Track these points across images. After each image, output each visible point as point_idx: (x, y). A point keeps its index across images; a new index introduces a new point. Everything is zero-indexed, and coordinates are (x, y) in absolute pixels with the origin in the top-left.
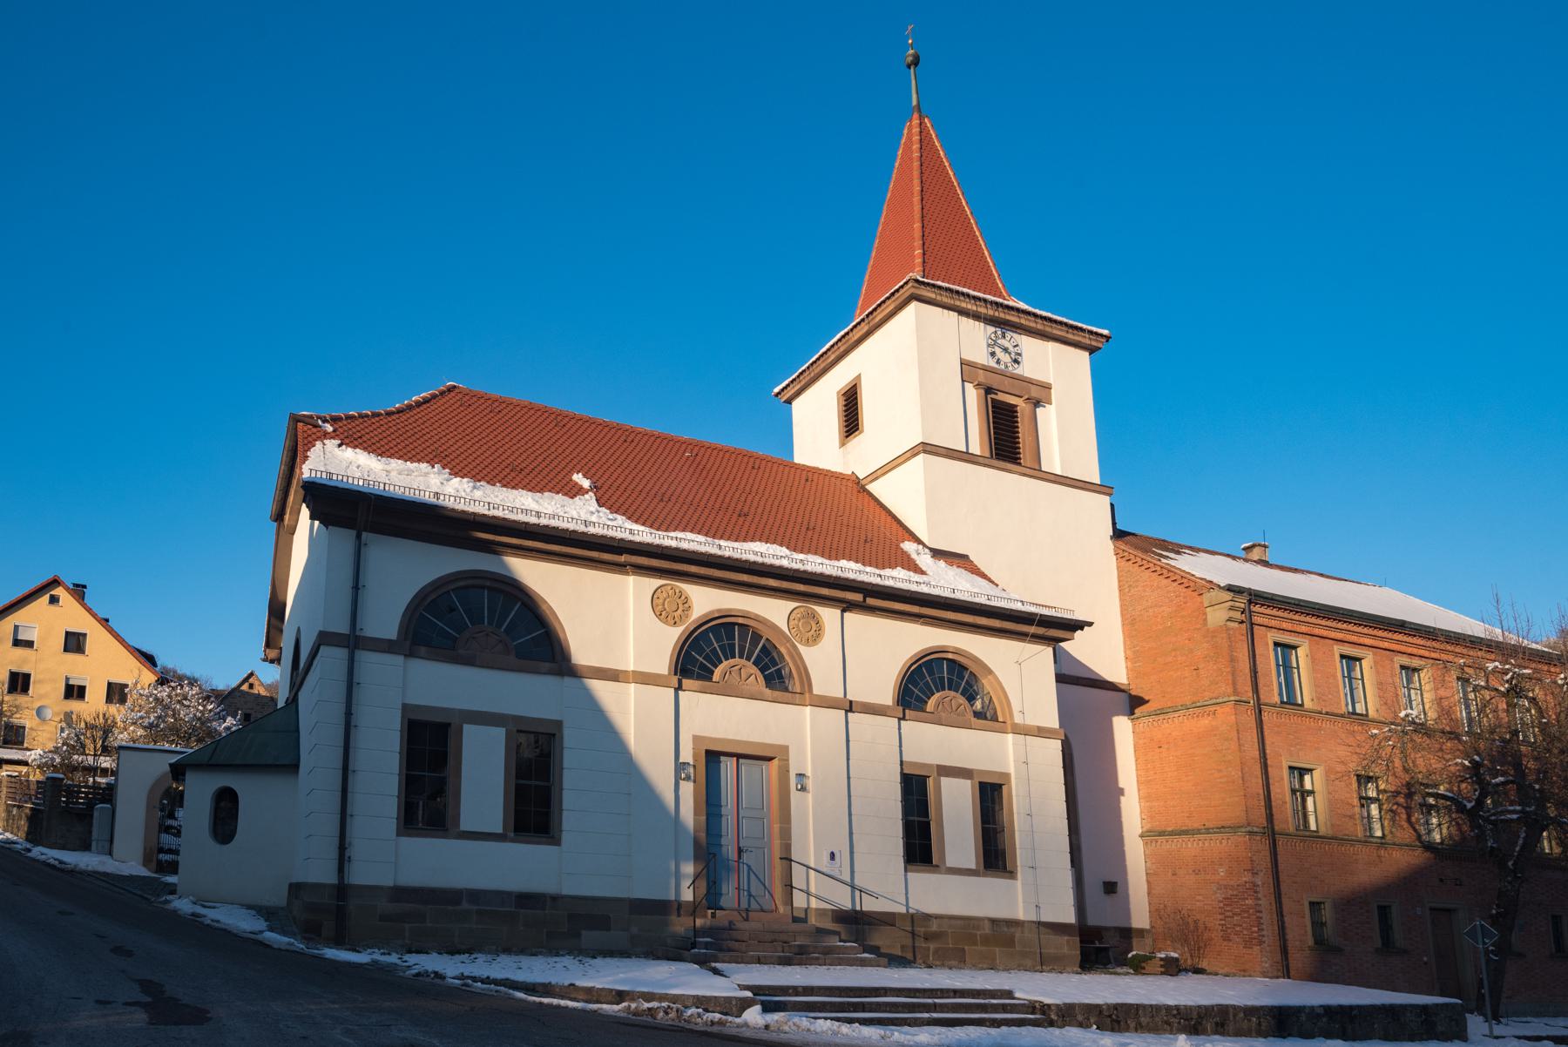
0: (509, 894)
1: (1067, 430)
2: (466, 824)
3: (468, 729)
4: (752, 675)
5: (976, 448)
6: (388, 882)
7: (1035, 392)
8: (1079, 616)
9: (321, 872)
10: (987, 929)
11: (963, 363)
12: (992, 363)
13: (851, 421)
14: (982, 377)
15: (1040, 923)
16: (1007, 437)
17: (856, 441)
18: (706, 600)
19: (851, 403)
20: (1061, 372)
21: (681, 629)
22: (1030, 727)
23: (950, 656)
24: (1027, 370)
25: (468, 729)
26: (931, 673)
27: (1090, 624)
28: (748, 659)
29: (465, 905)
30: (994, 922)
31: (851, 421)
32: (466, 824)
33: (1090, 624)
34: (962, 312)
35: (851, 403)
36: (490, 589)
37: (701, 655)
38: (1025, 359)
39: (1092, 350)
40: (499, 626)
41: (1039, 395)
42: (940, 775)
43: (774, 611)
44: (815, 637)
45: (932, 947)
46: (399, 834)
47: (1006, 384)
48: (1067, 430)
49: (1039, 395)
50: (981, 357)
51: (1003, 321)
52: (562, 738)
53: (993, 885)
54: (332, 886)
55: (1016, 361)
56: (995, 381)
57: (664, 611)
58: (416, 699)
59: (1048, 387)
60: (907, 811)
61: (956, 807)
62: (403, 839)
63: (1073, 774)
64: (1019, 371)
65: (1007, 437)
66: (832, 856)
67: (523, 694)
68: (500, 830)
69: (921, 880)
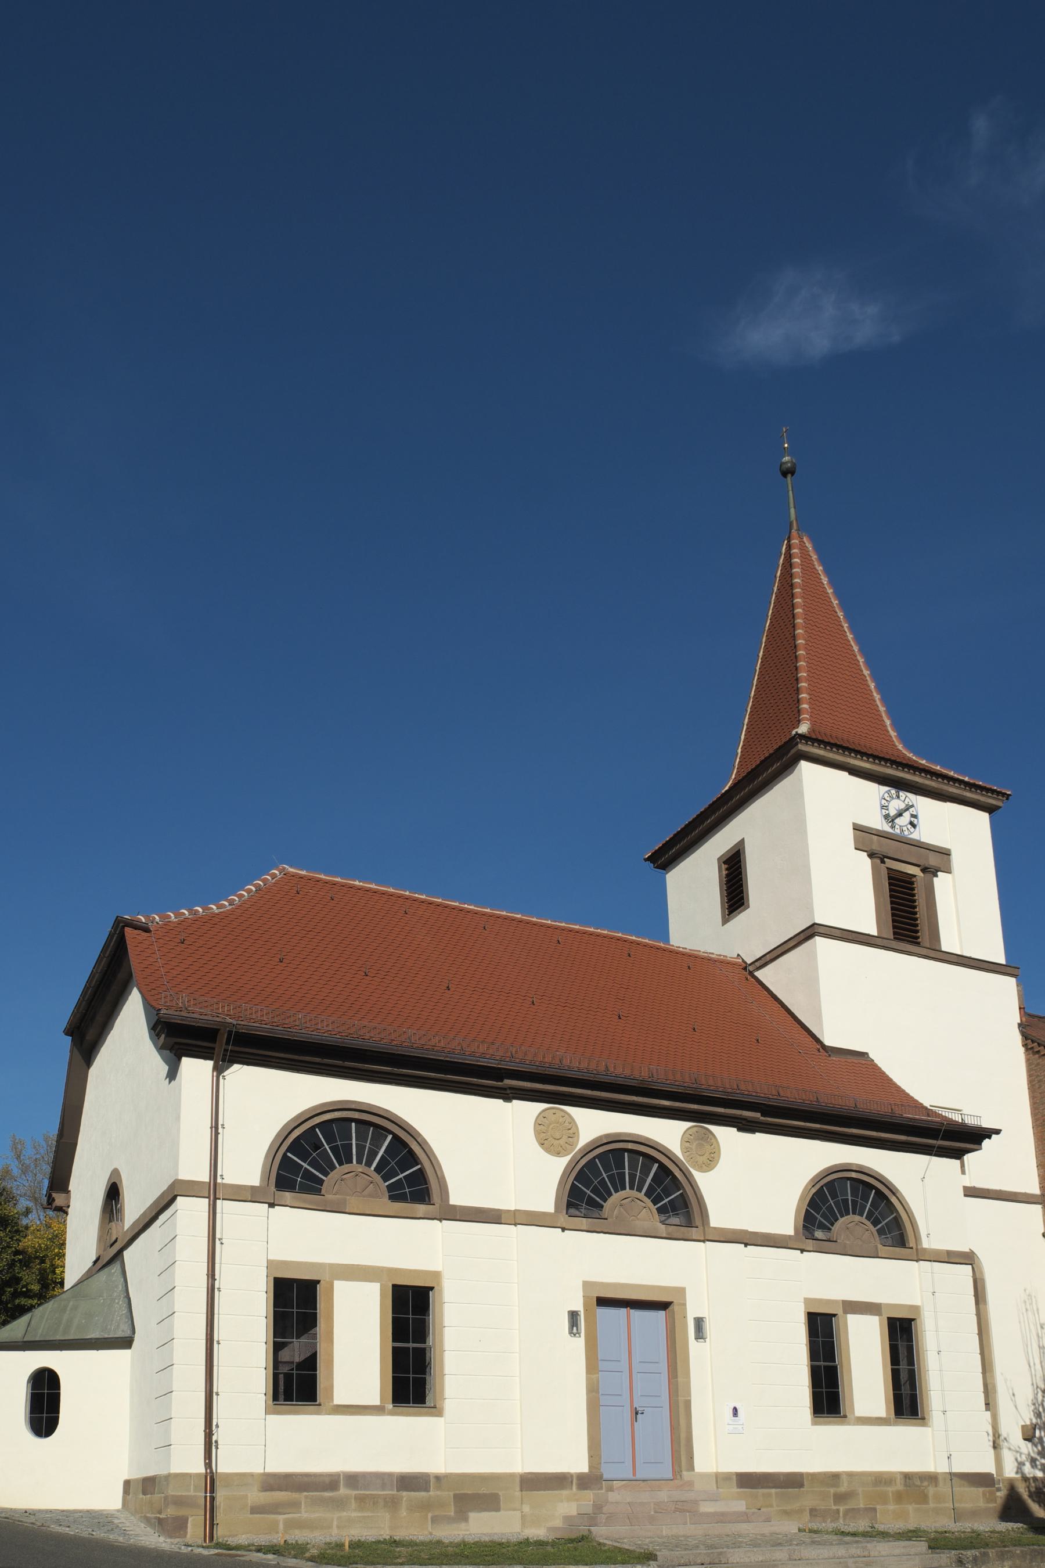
0: (390, 1475)
1: (968, 904)
2: (340, 1398)
3: (339, 1285)
4: (646, 1212)
5: (870, 927)
6: (259, 1470)
7: (933, 860)
8: (986, 1124)
9: (189, 1461)
10: (899, 1486)
11: (857, 828)
12: (887, 828)
13: (735, 896)
14: (876, 844)
15: (952, 1475)
16: (905, 917)
17: (741, 919)
18: (594, 1124)
19: (733, 867)
20: (959, 831)
21: (569, 1157)
22: (937, 1252)
23: (854, 1175)
24: (925, 834)
25: (882, 1413)
26: (834, 1196)
27: (997, 1132)
28: (639, 1190)
29: (343, 1491)
30: (907, 1477)
31: (735, 896)
32: (340, 1398)
33: (997, 1132)
34: (854, 772)
35: (733, 867)
36: (358, 1121)
37: (594, 1189)
38: (921, 822)
39: (990, 809)
40: (369, 1164)
41: (936, 860)
42: (846, 1312)
43: (667, 1134)
44: (710, 1162)
45: (842, 1509)
46: (268, 1412)
47: (903, 852)
48: (968, 904)
49: (936, 860)
50: (877, 822)
51: (896, 775)
52: (441, 1291)
53: (906, 1432)
54: (198, 1475)
55: (914, 825)
56: (889, 848)
57: (549, 1138)
58: (280, 1254)
59: (946, 853)
60: (814, 1355)
61: (864, 1351)
62: (270, 1417)
63: (816, 1375)
64: (915, 835)
65: (905, 917)
66: (735, 1411)
67: (406, 1243)
68: (378, 1403)
69: (831, 1431)
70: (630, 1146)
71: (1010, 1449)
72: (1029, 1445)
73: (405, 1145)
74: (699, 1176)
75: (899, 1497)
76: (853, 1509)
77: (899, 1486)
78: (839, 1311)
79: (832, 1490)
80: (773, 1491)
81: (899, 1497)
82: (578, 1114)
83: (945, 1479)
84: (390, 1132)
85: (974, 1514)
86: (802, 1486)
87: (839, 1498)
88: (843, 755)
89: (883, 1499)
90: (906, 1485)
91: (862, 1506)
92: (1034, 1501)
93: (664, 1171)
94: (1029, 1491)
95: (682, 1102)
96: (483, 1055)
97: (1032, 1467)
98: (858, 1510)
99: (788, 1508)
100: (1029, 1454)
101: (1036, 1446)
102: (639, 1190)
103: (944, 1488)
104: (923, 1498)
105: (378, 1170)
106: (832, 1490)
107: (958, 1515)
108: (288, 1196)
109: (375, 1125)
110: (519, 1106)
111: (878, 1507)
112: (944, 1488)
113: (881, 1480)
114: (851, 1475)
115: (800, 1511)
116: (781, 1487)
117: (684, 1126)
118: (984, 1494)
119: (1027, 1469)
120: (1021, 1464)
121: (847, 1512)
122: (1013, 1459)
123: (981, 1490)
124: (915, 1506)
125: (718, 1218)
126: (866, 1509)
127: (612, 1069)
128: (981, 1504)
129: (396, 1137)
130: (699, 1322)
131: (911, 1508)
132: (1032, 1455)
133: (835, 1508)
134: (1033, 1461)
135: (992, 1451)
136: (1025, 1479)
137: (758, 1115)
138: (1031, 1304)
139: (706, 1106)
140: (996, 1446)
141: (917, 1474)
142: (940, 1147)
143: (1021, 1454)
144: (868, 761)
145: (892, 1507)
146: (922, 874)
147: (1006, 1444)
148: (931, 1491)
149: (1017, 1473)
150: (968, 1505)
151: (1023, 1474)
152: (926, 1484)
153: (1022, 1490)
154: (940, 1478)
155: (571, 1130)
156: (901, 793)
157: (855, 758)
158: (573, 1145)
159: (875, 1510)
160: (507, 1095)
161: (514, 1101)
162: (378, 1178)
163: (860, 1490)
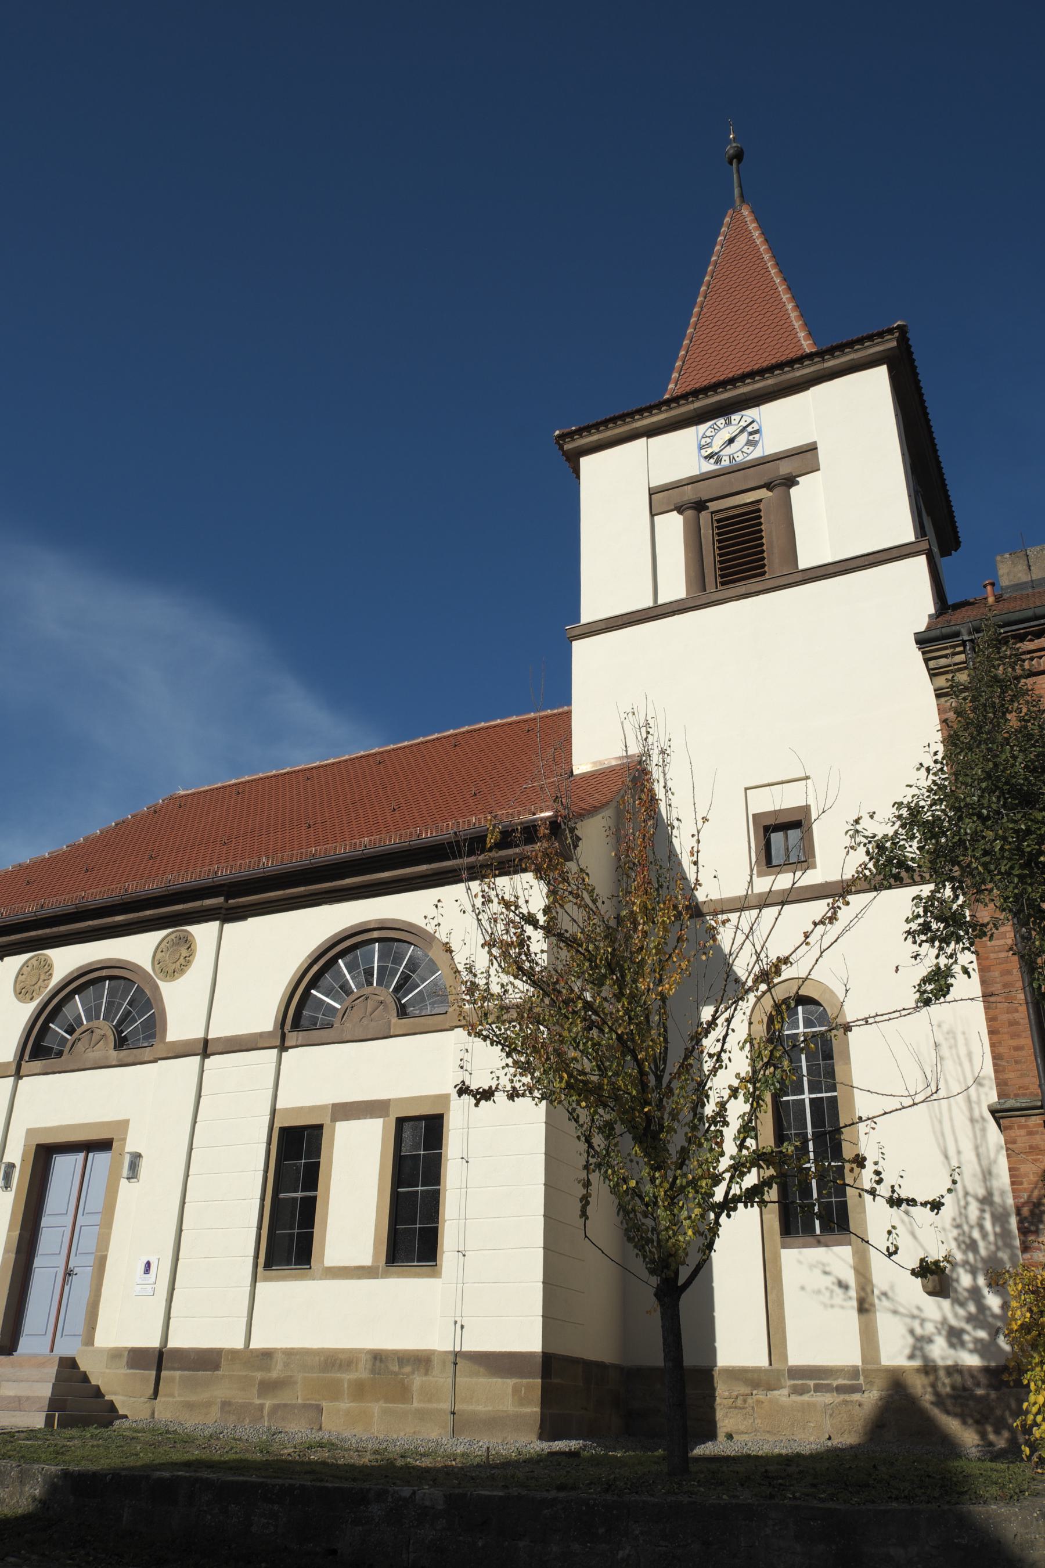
10: (362, 1373)
15: (457, 1357)
18: (67, 960)
30: (378, 1357)
34: (651, 432)
36: (111, 978)
42: (334, 1119)
43: (137, 949)
45: (268, 1403)
47: (737, 482)
53: (407, 1288)
71: (895, 1312)
72: (946, 1304)
75: (360, 1391)
76: (285, 1405)
77: (362, 1373)
78: (326, 1121)
79: (259, 1375)
80: (178, 1373)
81: (360, 1391)
83: (444, 1363)
85: (493, 1423)
86: (217, 1367)
87: (267, 1387)
88: (625, 423)
89: (334, 1391)
90: (373, 1371)
91: (300, 1401)
92: (948, 1413)
94: (937, 1394)
97: (952, 1345)
98: (293, 1406)
99: (193, 1398)
100: (944, 1321)
101: (962, 1304)
103: (441, 1378)
104: (403, 1393)
106: (259, 1375)
107: (457, 1422)
109: (393, 937)
111: (324, 1404)
112: (441, 1378)
113: (334, 1361)
114: (289, 1353)
115: (208, 1404)
116: (189, 1370)
117: (155, 937)
118: (516, 1390)
119: (940, 1351)
120: (921, 1342)
121: (275, 1409)
122: (903, 1331)
123: (511, 1382)
124: (382, 1404)
126: (305, 1407)
128: (508, 1406)
130: (136, 1157)
131: (376, 1408)
132: (953, 1322)
133: (258, 1402)
134: (954, 1336)
135: (854, 1314)
136: (929, 1369)
137: (221, 899)
138: (954, 1046)
140: (864, 1307)
141: (395, 1352)
142: (471, 868)
143: (923, 1321)
144: (661, 412)
145: (345, 1405)
146: (770, 494)
147: (885, 1303)
148: (418, 1381)
149: (911, 1357)
150: (481, 1408)
151: (925, 1358)
152: (407, 1369)
153: (919, 1386)
154: (436, 1361)
156: (733, 417)
157: (643, 418)
159: (319, 1410)
161: (6, 959)
163: (299, 1377)
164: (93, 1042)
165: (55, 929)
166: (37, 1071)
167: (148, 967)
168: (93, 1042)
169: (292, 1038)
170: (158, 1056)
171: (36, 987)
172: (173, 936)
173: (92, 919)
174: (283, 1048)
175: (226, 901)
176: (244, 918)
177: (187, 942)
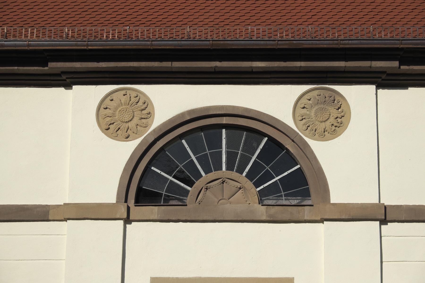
18: (170, 102)
36: (227, 127)
43: (276, 102)
57: (111, 124)
70: (225, 121)
73: (281, 146)
74: (316, 146)
82: (151, 91)
84: (265, 135)
93: (275, 146)
95: (285, 60)
96: (129, 37)
102: (240, 171)
105: (249, 176)
108: (153, 211)
109: (246, 128)
110: (79, 90)
117: (296, 90)
125: (340, 192)
127: (192, 36)
129: (271, 139)
137: (396, 64)
139: (324, 64)
155: (146, 109)
158: (146, 126)
160: (66, 80)
162: (249, 184)
164: (227, 194)
165: (412, 67)
166: (156, 218)
167: (289, 121)
168: (227, 194)
169: (137, 211)
170: (326, 217)
171: (132, 125)
172: (316, 92)
173: (220, 60)
174: (128, 221)
175: (400, 65)
176: (404, 86)
177: (339, 104)
